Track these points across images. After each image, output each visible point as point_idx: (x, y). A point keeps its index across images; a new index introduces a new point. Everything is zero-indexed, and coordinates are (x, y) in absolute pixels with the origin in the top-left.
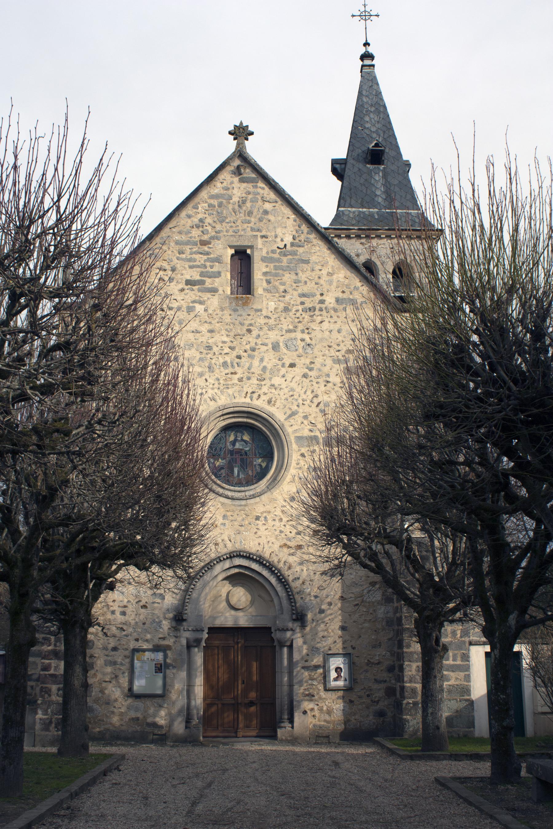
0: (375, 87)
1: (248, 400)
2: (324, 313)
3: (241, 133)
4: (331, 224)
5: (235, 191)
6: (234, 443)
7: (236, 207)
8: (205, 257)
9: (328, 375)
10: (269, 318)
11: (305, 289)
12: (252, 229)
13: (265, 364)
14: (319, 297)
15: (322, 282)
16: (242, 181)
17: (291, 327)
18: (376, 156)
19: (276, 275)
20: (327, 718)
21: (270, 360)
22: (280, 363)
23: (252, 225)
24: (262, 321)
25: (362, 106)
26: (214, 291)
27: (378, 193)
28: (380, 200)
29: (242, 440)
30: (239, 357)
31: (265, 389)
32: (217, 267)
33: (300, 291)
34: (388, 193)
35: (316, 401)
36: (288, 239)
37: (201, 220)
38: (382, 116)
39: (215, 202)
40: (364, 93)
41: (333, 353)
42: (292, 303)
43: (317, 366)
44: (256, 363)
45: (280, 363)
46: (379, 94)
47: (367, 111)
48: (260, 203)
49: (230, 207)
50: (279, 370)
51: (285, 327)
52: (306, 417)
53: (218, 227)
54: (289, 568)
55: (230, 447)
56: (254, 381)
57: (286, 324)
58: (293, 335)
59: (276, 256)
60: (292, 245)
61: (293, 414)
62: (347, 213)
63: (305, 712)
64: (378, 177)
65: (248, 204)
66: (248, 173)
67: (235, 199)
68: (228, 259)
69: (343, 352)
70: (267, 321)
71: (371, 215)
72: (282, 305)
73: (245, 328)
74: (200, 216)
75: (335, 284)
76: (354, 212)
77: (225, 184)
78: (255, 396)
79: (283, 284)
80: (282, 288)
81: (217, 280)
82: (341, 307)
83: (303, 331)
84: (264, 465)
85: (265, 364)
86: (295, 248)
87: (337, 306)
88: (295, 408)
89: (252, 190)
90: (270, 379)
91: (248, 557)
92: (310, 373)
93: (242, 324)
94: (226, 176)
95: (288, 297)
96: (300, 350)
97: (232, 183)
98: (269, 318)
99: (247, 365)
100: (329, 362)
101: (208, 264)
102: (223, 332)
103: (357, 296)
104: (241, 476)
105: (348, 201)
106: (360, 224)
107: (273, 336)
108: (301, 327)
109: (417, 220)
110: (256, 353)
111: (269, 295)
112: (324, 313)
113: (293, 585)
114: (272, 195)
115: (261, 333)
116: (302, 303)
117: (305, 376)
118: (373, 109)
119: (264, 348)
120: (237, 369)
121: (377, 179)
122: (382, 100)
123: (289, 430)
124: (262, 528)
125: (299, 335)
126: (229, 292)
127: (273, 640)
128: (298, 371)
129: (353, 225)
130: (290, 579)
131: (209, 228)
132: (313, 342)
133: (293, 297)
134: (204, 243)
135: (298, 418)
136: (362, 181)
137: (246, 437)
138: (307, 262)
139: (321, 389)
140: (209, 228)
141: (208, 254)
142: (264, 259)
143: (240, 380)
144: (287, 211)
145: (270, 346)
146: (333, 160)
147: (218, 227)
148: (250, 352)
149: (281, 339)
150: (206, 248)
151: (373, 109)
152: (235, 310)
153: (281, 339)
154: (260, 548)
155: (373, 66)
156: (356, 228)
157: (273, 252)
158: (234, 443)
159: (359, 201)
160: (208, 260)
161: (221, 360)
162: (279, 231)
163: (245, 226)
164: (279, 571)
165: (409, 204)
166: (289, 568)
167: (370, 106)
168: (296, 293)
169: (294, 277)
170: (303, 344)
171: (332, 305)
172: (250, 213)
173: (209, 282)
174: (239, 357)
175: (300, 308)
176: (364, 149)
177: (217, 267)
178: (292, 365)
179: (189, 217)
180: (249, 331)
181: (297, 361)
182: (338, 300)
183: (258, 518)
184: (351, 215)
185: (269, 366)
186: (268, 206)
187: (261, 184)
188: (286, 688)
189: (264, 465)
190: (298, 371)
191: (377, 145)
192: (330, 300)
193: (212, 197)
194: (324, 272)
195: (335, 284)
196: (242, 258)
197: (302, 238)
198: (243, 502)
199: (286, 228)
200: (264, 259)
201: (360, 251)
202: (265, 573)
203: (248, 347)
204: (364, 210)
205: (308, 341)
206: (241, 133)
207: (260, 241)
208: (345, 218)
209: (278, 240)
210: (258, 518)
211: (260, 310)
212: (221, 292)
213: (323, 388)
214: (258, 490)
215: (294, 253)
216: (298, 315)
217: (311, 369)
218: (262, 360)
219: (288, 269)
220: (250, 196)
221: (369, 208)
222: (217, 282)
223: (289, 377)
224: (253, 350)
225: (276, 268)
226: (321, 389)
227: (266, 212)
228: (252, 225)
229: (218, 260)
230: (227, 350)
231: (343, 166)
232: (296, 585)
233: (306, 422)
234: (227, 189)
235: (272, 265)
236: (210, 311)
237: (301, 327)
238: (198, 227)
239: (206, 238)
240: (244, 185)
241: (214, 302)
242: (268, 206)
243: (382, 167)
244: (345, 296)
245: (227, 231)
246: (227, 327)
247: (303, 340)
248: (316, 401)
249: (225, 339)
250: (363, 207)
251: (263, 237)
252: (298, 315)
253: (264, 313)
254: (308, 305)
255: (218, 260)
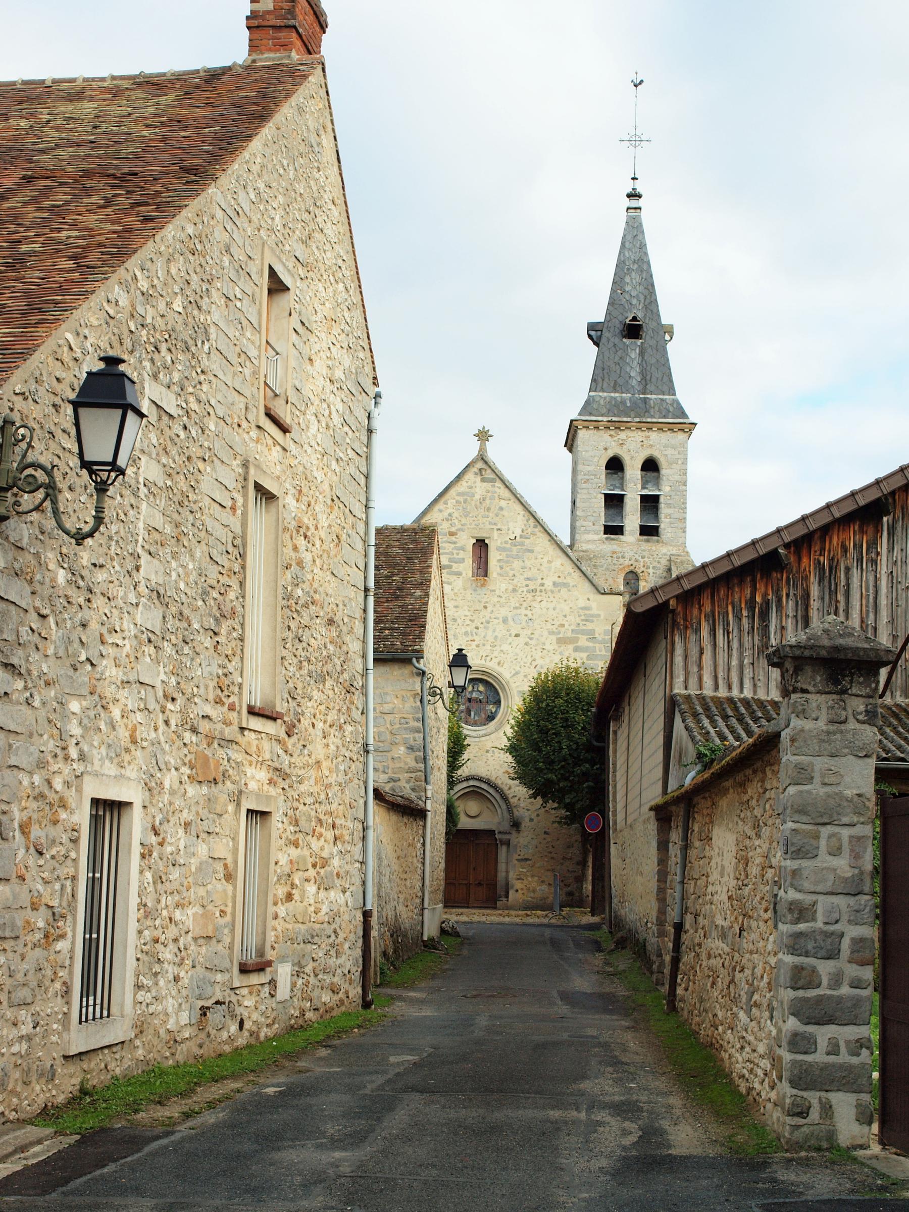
0: (640, 237)
1: (483, 662)
2: (543, 594)
3: (483, 436)
4: (580, 414)
5: (477, 490)
6: (471, 693)
7: (478, 503)
8: (453, 546)
9: (544, 644)
10: (500, 597)
11: (529, 574)
12: (490, 523)
13: (496, 634)
14: (540, 581)
15: (542, 568)
16: (483, 480)
17: (517, 605)
18: (633, 331)
19: (507, 562)
20: (532, 895)
21: (501, 630)
22: (508, 633)
23: (489, 519)
24: (496, 599)
25: (624, 262)
26: (459, 574)
27: (633, 374)
28: (634, 383)
29: (478, 691)
30: (477, 628)
31: (496, 654)
32: (462, 555)
33: (525, 576)
34: (643, 374)
35: (534, 664)
36: (518, 533)
37: (450, 515)
38: (644, 275)
39: (461, 499)
40: (627, 245)
41: (549, 626)
42: (519, 585)
43: (535, 636)
44: (490, 633)
45: (508, 633)
46: (643, 246)
47: (628, 269)
48: (497, 500)
49: (473, 503)
50: (507, 639)
51: (513, 605)
52: (526, 676)
53: (464, 521)
54: (510, 789)
55: (469, 696)
56: (488, 647)
57: (514, 602)
58: (518, 611)
59: (508, 546)
60: (521, 537)
61: (517, 673)
62: (597, 399)
63: (517, 891)
64: (634, 354)
65: (488, 501)
66: (489, 474)
67: (477, 497)
68: (470, 548)
69: (556, 626)
70: (499, 599)
71: (623, 402)
72: (511, 588)
73: (483, 604)
74: (450, 511)
75: (553, 570)
76: (605, 398)
77: (469, 483)
78: (489, 658)
79: (512, 570)
80: (511, 573)
81: (461, 565)
82: (557, 589)
83: (526, 609)
84: (494, 710)
85: (496, 634)
86: (522, 540)
87: (553, 589)
88: (518, 668)
89: (491, 489)
90: (500, 646)
91: (480, 779)
92: (530, 642)
93: (480, 602)
94: (470, 476)
95: (516, 580)
96: (524, 624)
97: (475, 482)
98: (500, 597)
99: (483, 634)
100: (545, 633)
101: (455, 552)
102: (466, 608)
103: (569, 580)
104: (476, 718)
105: (600, 385)
106: (611, 414)
107: (504, 612)
108: (525, 604)
109: (671, 409)
110: (490, 625)
111: (501, 578)
112: (543, 594)
113: (512, 801)
114: (507, 494)
115: (494, 609)
116: (527, 586)
117: (526, 644)
118: (636, 266)
119: (497, 621)
120: (475, 637)
121: (633, 357)
122: (646, 254)
123: (513, 686)
124: (491, 759)
125: (524, 612)
126: (471, 575)
127: (496, 840)
128: (522, 640)
129: (602, 415)
130: (510, 796)
131: (456, 521)
132: (534, 618)
133: (520, 581)
134: (452, 534)
135: (521, 676)
136: (617, 359)
137: (481, 688)
138: (532, 551)
139: (538, 655)
140: (456, 521)
141: (455, 543)
142: (498, 549)
143: (478, 646)
144: (519, 508)
145: (501, 619)
146: (589, 324)
147: (464, 521)
148: (485, 624)
149: (510, 615)
150: (453, 538)
151: (636, 266)
152: (475, 590)
153: (510, 615)
154: (489, 773)
155: (640, 208)
156: (605, 419)
157: (506, 542)
158: (471, 693)
159: (612, 385)
160: (455, 548)
161: (464, 630)
162: (511, 525)
163: (485, 520)
164: (502, 791)
165: (665, 388)
166: (510, 789)
167: (633, 265)
168: (522, 577)
169: (521, 563)
170: (526, 618)
171: (550, 588)
172: (489, 509)
173: (455, 565)
174: (477, 628)
175: (525, 589)
176: (621, 318)
177: (462, 555)
178: (517, 635)
179: (441, 511)
180: (485, 607)
181: (521, 632)
182: (554, 584)
183: (487, 751)
184: (602, 402)
185: (500, 636)
186: (503, 503)
187: (498, 484)
188: (504, 874)
189: (494, 710)
190: (522, 640)
191: (634, 319)
192: (548, 583)
193: (459, 494)
194: (545, 560)
195: (553, 570)
196: (481, 545)
197: (530, 530)
198: (477, 739)
199: (517, 523)
200: (498, 549)
201: (608, 444)
202: (491, 791)
203: (484, 620)
204: (617, 395)
205: (530, 616)
206: (483, 436)
207: (496, 533)
208: (595, 406)
209: (510, 532)
210: (487, 751)
211: (494, 591)
212: (464, 575)
213: (540, 654)
214: (489, 730)
215: (522, 544)
216: (523, 595)
217: (531, 639)
218: (494, 631)
219: (517, 557)
220: (489, 494)
221: (622, 393)
222: (460, 567)
223: (514, 644)
224: (488, 622)
225: (507, 556)
226: (538, 655)
227: (501, 509)
228: (489, 519)
229: (463, 549)
230: (468, 622)
231: (599, 333)
232: (514, 801)
233: (526, 680)
234: (471, 488)
235: (504, 554)
236: (456, 591)
237: (525, 604)
238: (447, 520)
239: (453, 529)
240: (485, 484)
241: (459, 583)
242: (503, 503)
243: (639, 342)
244: (560, 580)
245: (470, 524)
246: (469, 604)
247: (526, 615)
248: (534, 664)
249: (467, 613)
250: (615, 391)
251: (498, 529)
252: (523, 595)
253: (497, 593)
254: (531, 587)
255: (463, 549)
